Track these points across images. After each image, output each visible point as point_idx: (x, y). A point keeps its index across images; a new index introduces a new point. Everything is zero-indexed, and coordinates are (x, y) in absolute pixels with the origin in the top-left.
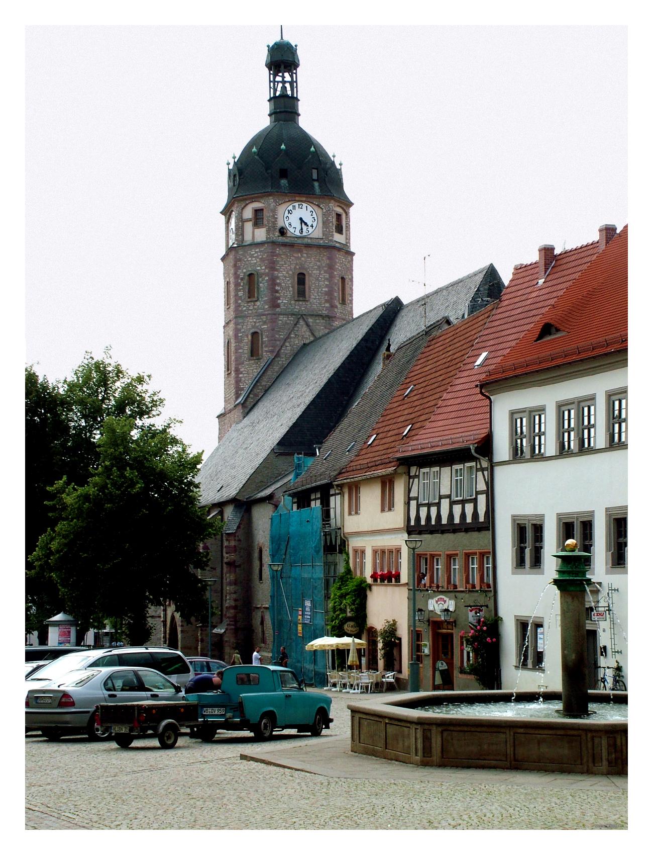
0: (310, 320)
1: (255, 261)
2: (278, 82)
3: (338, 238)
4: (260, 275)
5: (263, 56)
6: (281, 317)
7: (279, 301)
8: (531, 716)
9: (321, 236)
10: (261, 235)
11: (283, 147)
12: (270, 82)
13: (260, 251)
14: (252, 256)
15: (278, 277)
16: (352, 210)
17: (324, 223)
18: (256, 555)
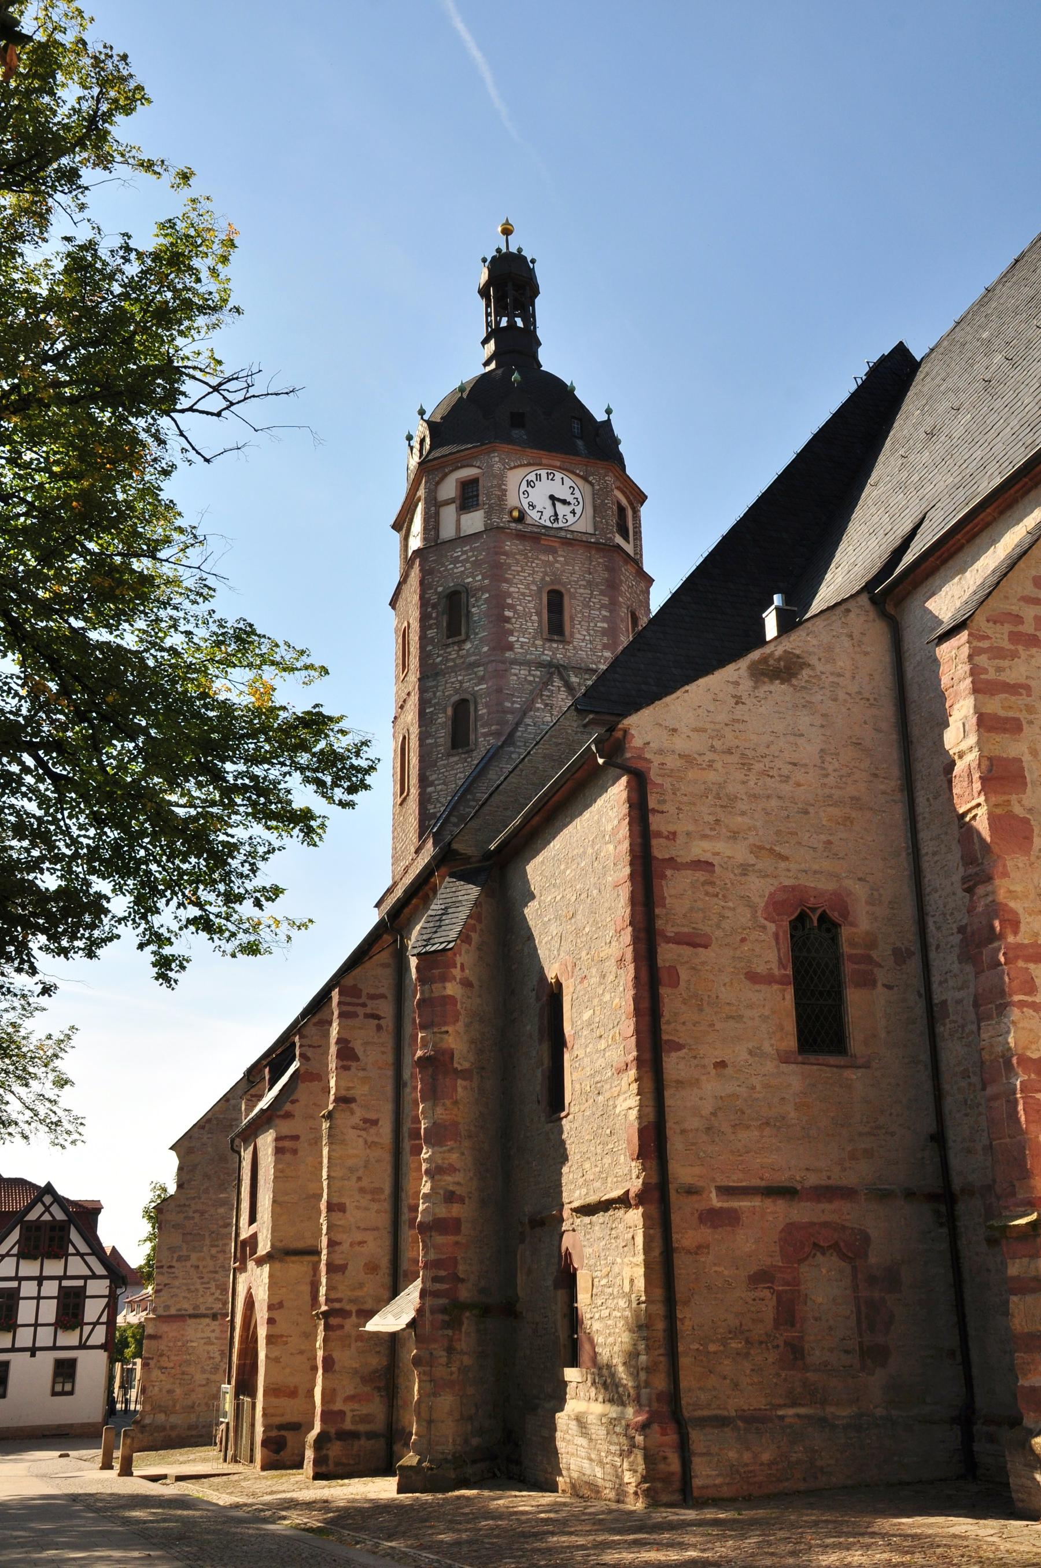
3: (619, 540)
4: (468, 591)
6: (515, 669)
7: (512, 639)
8: (349, 1485)
9: (591, 530)
13: (472, 550)
15: (510, 595)
17: (595, 508)
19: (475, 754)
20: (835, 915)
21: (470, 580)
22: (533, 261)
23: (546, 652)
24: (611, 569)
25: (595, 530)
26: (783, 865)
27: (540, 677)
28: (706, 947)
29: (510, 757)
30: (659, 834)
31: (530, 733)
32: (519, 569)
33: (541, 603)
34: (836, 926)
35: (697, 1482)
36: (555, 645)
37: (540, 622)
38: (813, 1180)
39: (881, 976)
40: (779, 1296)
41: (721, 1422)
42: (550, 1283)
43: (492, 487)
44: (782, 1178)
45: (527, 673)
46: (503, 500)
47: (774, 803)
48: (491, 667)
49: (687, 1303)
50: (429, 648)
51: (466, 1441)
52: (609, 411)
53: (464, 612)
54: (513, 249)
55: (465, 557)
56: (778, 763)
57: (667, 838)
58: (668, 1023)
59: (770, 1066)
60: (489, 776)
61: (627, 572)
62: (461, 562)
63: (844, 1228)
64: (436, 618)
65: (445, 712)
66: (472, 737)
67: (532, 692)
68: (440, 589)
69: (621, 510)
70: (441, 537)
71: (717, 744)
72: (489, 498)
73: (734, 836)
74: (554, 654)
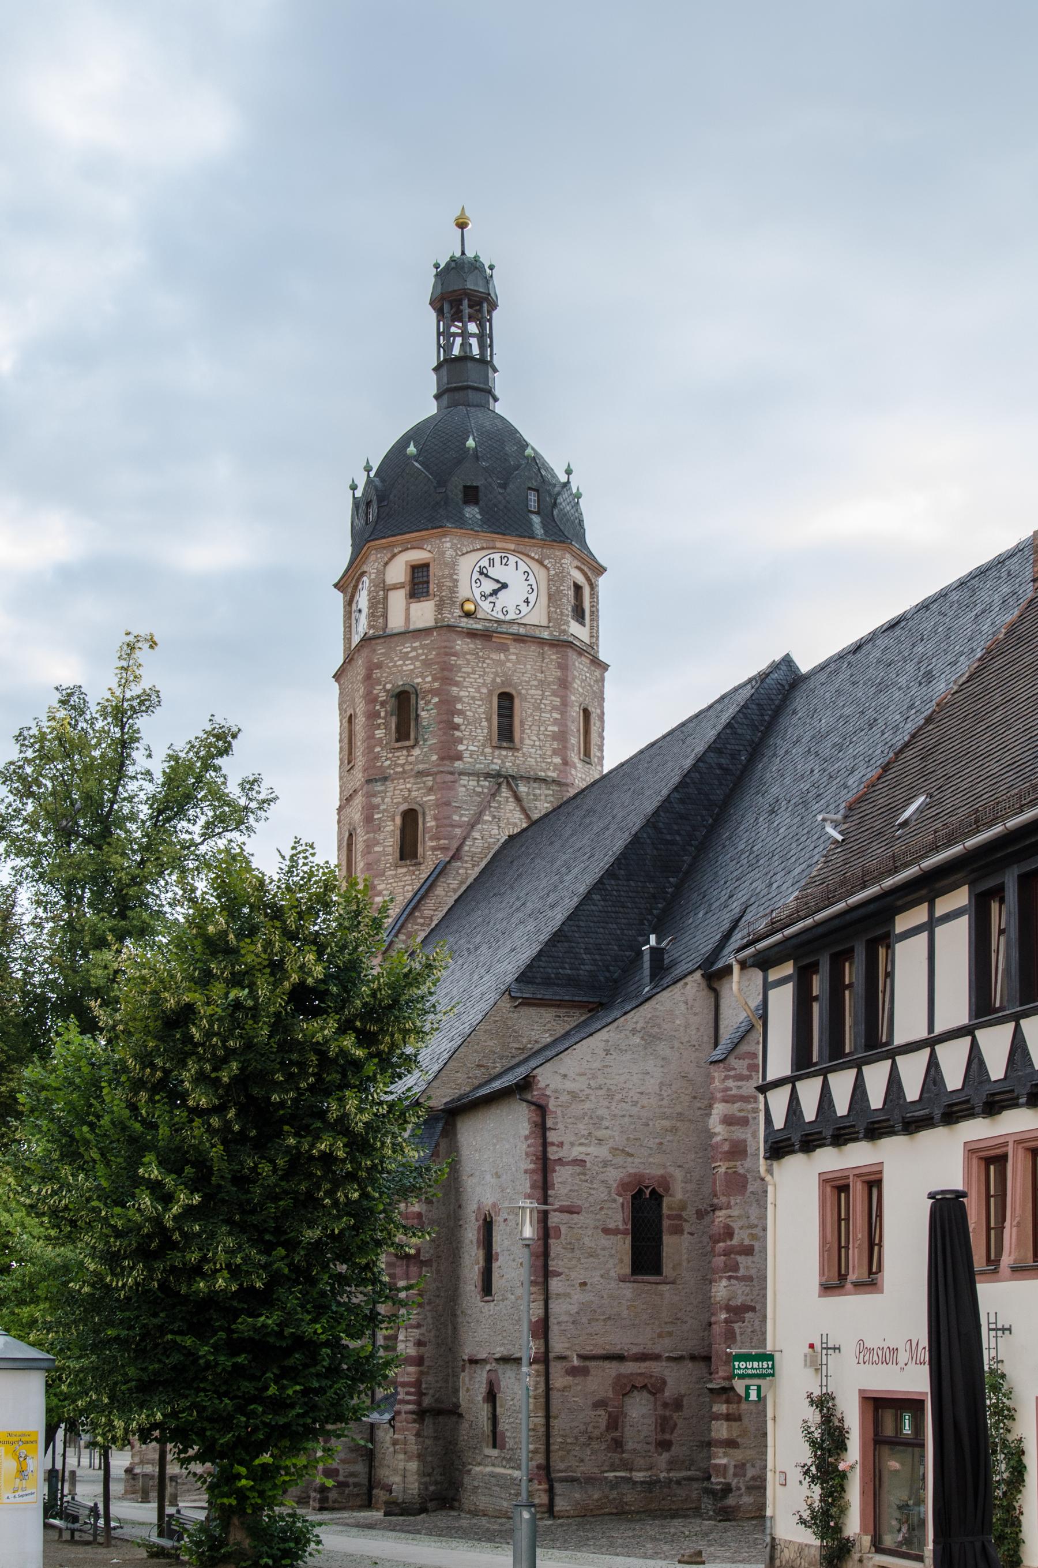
0: (523, 789)
1: (407, 667)
2: (455, 335)
3: (575, 629)
5: (426, 284)
6: (464, 780)
7: (461, 747)
9: (544, 623)
10: (424, 614)
11: (471, 443)
12: (439, 334)
13: (422, 647)
14: (405, 657)
15: (459, 699)
16: (602, 581)
17: (550, 597)
18: (471, 1234)
19: (423, 867)
20: (660, 1190)
21: (419, 680)
22: (491, 268)
23: (495, 761)
24: (563, 667)
25: (549, 621)
26: (630, 1159)
27: (489, 788)
28: (578, 1213)
29: (457, 873)
30: (553, 1144)
31: (477, 847)
32: (470, 670)
33: (491, 707)
34: (662, 1197)
35: (556, 1509)
36: (504, 753)
37: (490, 727)
38: (635, 1350)
39: (687, 1227)
40: (610, 1414)
41: (572, 1480)
42: (480, 1398)
43: (443, 577)
44: (616, 1350)
45: (475, 783)
46: (455, 592)
47: (626, 1119)
48: (439, 778)
49: (556, 1418)
50: (378, 749)
51: (427, 1489)
52: (569, 472)
53: (413, 716)
54: (470, 254)
55: (414, 654)
56: (631, 1093)
57: (558, 1146)
58: (553, 1260)
59: (613, 1285)
60: (436, 893)
61: (580, 666)
62: (411, 659)
63: (651, 1376)
64: (385, 718)
65: (393, 820)
66: (420, 850)
67: (481, 803)
68: (389, 686)
69: (578, 588)
70: (390, 625)
71: (592, 1083)
72: (440, 589)
73: (600, 1141)
74: (503, 762)
